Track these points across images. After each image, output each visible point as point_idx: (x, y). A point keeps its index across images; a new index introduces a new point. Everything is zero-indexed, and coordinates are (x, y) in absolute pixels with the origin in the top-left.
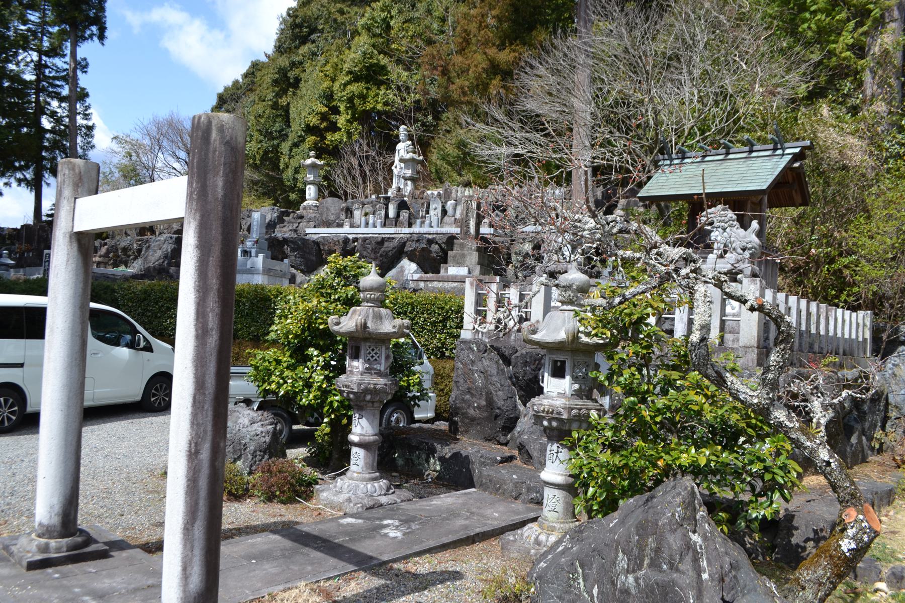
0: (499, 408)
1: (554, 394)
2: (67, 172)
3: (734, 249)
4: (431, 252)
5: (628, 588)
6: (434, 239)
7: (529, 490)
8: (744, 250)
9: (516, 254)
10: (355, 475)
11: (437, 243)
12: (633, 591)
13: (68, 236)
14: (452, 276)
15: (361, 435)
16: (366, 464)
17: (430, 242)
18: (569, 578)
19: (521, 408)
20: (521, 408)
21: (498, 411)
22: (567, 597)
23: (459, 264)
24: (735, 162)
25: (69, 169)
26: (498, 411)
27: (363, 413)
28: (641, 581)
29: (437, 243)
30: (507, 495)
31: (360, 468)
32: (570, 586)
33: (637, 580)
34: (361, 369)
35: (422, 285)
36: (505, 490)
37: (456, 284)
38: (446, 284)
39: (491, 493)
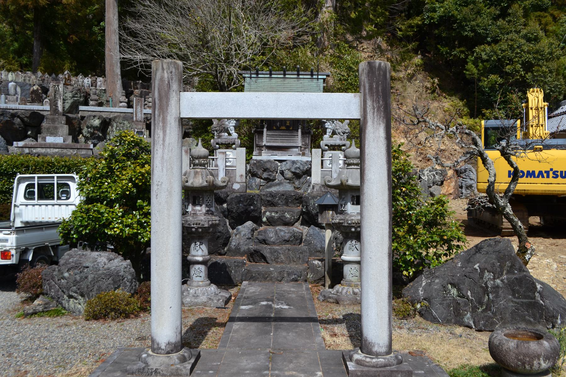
0: (220, 232)
1: (356, 213)
2: (174, 70)
3: (339, 133)
4: (14, 124)
5: (498, 285)
6: (16, 113)
7: (289, 274)
8: (344, 133)
9: (88, 127)
10: (201, 283)
11: (19, 117)
12: (501, 286)
13: (177, 120)
14: (50, 144)
15: (202, 256)
16: (205, 275)
17: (14, 116)
18: (444, 294)
19: (231, 230)
20: (231, 230)
21: (219, 234)
22: (445, 302)
23: (54, 133)
24: (263, 80)
25: (175, 68)
26: (219, 234)
27: (203, 241)
28: (505, 281)
29: (19, 117)
30: (274, 280)
31: (202, 278)
32: (445, 297)
33: (502, 281)
34: (204, 211)
35: (27, 151)
36: (272, 277)
37: (57, 150)
38: (48, 150)
39: (261, 281)
